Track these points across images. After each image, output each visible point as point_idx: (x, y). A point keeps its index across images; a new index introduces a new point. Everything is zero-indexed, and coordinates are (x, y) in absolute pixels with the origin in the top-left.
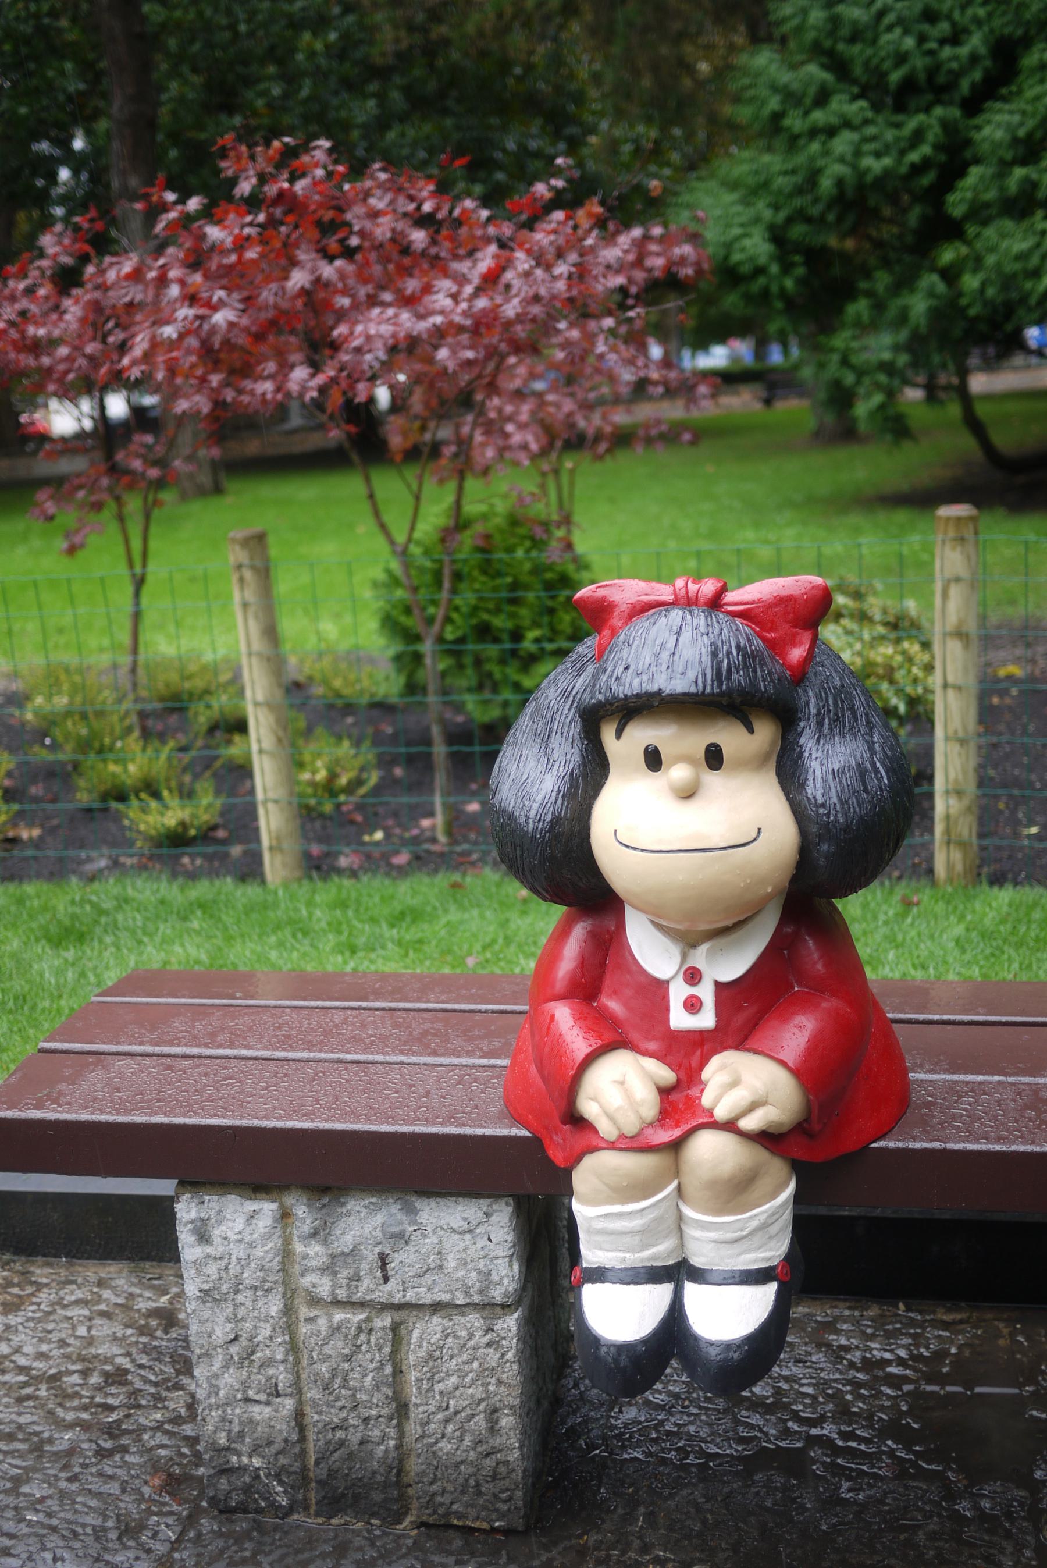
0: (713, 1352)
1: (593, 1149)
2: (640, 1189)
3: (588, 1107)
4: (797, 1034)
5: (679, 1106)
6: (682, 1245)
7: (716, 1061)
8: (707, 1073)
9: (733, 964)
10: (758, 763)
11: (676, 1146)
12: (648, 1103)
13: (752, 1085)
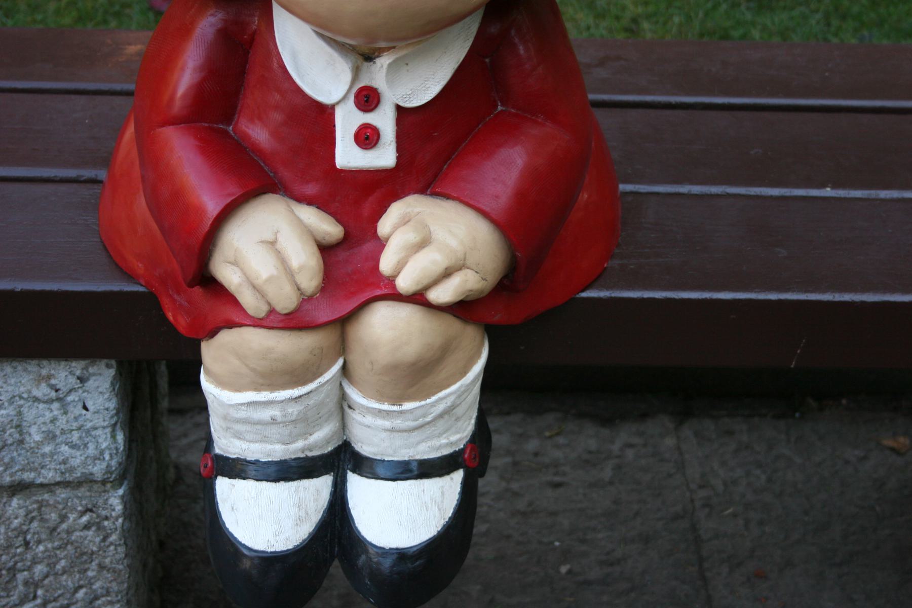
1: (231, 325)
2: (297, 374)
3: (226, 273)
4: (507, 169)
5: (350, 276)
7: (396, 211)
8: (384, 226)
9: (421, 82)
11: (344, 322)
12: (305, 262)
13: (438, 243)
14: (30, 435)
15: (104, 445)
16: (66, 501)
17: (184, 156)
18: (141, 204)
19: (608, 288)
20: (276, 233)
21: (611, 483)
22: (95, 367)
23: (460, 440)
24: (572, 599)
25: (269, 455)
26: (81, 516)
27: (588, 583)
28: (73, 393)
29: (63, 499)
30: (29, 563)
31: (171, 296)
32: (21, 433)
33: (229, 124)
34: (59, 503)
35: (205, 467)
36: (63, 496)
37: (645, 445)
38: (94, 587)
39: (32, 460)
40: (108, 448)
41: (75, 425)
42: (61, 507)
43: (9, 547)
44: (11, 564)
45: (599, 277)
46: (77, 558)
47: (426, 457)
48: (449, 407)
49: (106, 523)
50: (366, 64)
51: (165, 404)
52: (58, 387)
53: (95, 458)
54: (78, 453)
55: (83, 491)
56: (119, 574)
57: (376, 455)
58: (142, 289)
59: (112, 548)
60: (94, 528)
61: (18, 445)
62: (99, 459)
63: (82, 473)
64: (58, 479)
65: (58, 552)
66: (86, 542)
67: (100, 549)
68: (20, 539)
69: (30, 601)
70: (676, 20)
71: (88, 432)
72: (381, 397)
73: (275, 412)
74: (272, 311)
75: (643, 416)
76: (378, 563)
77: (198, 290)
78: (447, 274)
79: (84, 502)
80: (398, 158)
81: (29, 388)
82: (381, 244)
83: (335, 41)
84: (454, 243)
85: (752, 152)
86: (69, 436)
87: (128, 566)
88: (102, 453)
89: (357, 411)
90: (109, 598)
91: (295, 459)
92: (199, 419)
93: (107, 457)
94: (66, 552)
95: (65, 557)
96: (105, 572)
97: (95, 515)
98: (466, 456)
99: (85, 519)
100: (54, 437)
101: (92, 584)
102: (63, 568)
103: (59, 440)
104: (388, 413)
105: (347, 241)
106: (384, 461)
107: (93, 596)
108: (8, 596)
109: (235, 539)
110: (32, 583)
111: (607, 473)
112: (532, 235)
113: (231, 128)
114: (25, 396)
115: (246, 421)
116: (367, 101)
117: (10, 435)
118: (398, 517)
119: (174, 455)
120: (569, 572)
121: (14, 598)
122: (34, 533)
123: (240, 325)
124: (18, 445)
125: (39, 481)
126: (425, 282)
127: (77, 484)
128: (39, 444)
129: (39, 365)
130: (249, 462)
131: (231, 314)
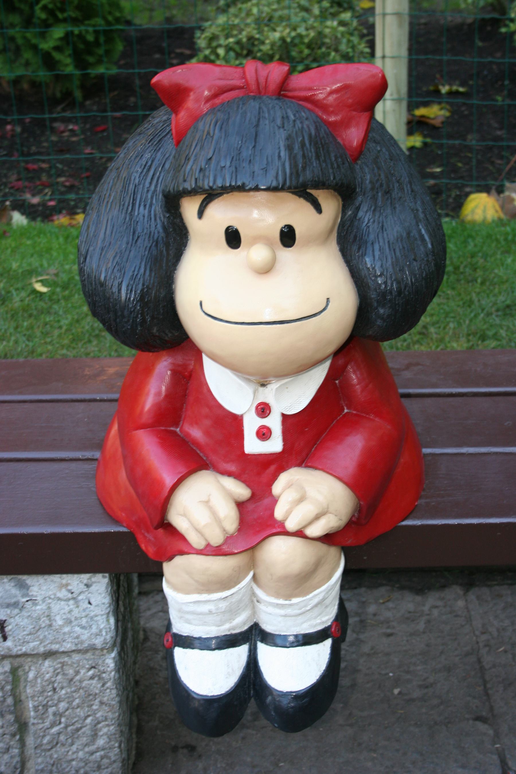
0: (285, 702)
1: (182, 553)
3: (177, 518)
4: (351, 449)
5: (256, 522)
6: (254, 613)
8: (277, 488)
9: (297, 396)
10: (325, 239)
12: (229, 518)
13: (313, 498)
14: (56, 621)
15: (102, 626)
16: (78, 662)
17: (150, 449)
18: (123, 475)
19: (419, 518)
20: (210, 495)
21: (424, 633)
22: (96, 578)
23: (328, 620)
24: (402, 712)
25: (208, 634)
26: (88, 671)
27: (413, 700)
29: (77, 660)
30: (56, 702)
31: (143, 534)
32: (50, 620)
33: (177, 427)
34: (74, 663)
35: (168, 641)
36: (77, 658)
37: (445, 606)
38: (97, 716)
39: (57, 637)
40: (104, 628)
41: (84, 614)
42: (75, 665)
43: (43, 692)
44: (45, 702)
45: (411, 513)
46: (86, 697)
47: (307, 632)
48: (321, 600)
49: (104, 675)
50: (261, 389)
51: (136, 591)
52: (73, 591)
53: (97, 635)
54: (86, 632)
55: (89, 655)
56: (113, 707)
57: (275, 631)
59: (108, 691)
60: (96, 679)
61: (48, 627)
62: (99, 635)
63: (89, 644)
64: (74, 648)
65: (74, 694)
66: (92, 687)
67: (101, 692)
68: (50, 686)
69: (57, 725)
70: (451, 325)
71: (92, 618)
72: (278, 595)
73: (211, 607)
74: (208, 545)
75: (443, 587)
76: (279, 701)
77: (161, 531)
78: (317, 517)
79: (90, 662)
80: (284, 445)
81: (55, 592)
82: (275, 501)
84: (320, 498)
85: (506, 424)
86: (80, 621)
87: (118, 702)
88: (101, 631)
89: (263, 604)
90: (107, 723)
92: (158, 598)
93: (104, 633)
94: (79, 694)
95: (79, 697)
96: (104, 706)
97: (97, 671)
98: (333, 630)
99: (91, 673)
100: (71, 622)
101: (96, 714)
102: (78, 704)
103: (74, 624)
104: (282, 606)
106: (280, 635)
107: (96, 722)
108: (43, 723)
109: (188, 688)
110: (58, 714)
111: (421, 626)
112: (371, 488)
113: (178, 430)
114: (52, 597)
115: (193, 613)
116: (263, 412)
117: (44, 621)
118: (292, 671)
119: (142, 622)
120: (400, 693)
121: (47, 724)
122: (59, 683)
123: (188, 553)
124: (48, 627)
125: (61, 650)
126: (303, 524)
127: (85, 651)
128: (61, 626)
129: (60, 578)
130: (195, 638)
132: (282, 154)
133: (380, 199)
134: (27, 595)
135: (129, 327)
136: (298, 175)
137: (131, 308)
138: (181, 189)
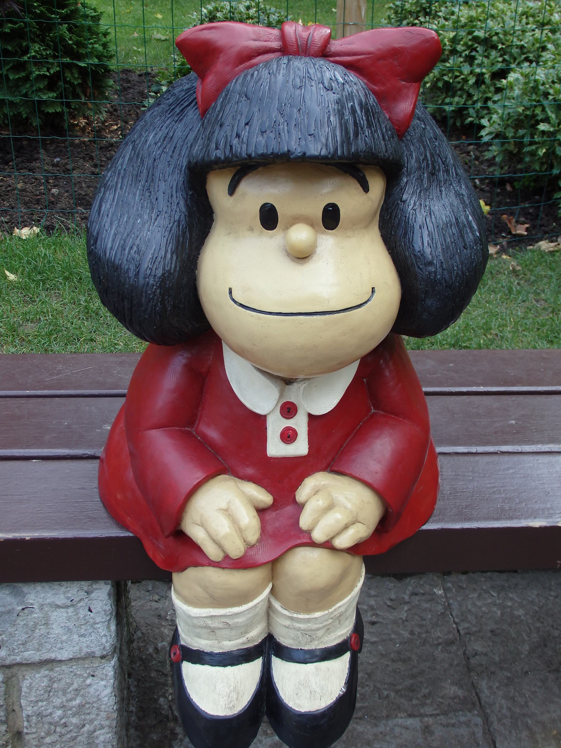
1: (196, 565)
3: (196, 533)
5: (282, 528)
6: (269, 624)
9: (325, 399)
12: (249, 521)
13: (339, 506)
23: (347, 631)
28: (82, 601)
35: (175, 654)
58: (131, 535)
82: (300, 507)
83: (268, 373)
91: (238, 650)
105: (274, 506)
118: (310, 688)
123: (203, 565)
126: (332, 535)
131: (200, 559)
132: (332, 119)
133: (425, 181)
134: (22, 602)
135: (147, 316)
136: (349, 144)
137: (150, 294)
138: (213, 158)
